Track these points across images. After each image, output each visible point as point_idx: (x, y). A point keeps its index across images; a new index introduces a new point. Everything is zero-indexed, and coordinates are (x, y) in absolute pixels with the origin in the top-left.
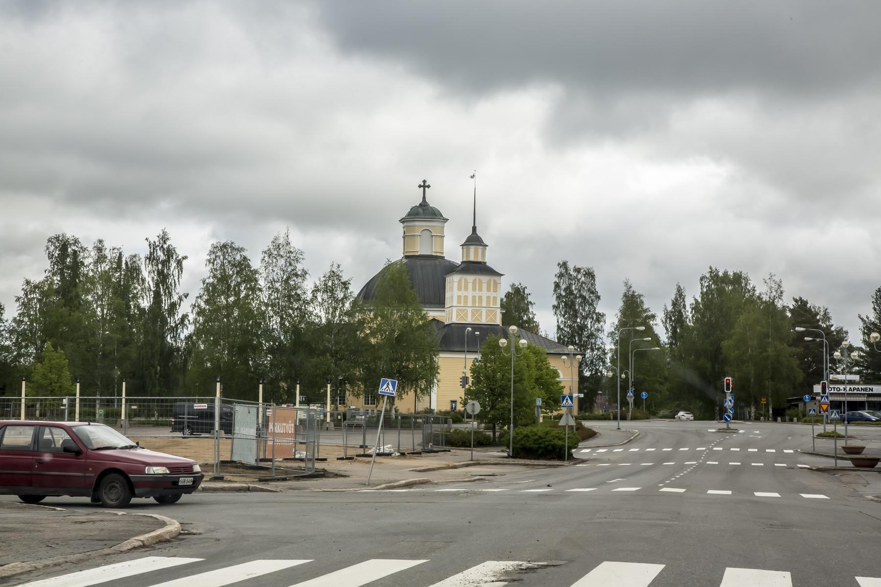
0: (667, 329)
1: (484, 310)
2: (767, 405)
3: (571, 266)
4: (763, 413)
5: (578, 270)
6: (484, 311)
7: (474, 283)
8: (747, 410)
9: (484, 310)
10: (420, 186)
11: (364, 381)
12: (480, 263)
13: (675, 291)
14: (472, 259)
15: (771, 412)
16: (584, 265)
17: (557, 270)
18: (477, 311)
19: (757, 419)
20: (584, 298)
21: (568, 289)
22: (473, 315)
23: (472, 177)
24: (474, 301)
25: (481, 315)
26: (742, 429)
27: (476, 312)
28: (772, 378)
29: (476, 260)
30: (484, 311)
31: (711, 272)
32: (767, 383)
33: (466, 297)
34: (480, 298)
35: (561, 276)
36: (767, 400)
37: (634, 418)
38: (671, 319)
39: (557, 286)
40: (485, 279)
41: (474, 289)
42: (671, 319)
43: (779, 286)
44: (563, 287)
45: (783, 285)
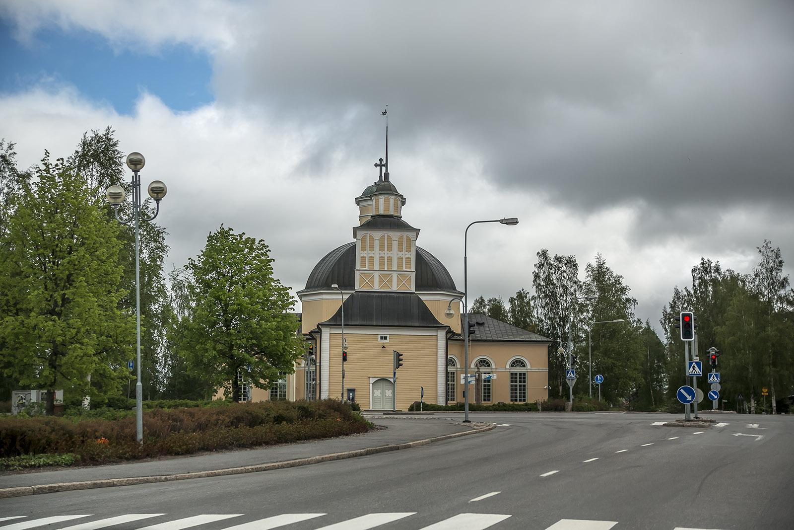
0: (666, 330)
1: (395, 275)
2: (769, 398)
3: (551, 255)
4: (764, 409)
5: (559, 259)
6: (395, 276)
7: (382, 240)
8: (746, 406)
9: (395, 275)
10: (376, 165)
11: (57, 346)
12: (392, 216)
13: (673, 294)
14: (381, 212)
15: (774, 404)
16: (565, 254)
17: (537, 260)
18: (386, 276)
19: (759, 411)
20: (565, 288)
21: (548, 280)
22: (381, 281)
23: (384, 114)
24: (382, 264)
25: (391, 281)
26: (723, 421)
27: (385, 277)
28: (774, 364)
29: (387, 213)
30: (395, 276)
31: (703, 264)
32: (768, 369)
33: (372, 258)
34: (390, 259)
35: (541, 266)
36: (769, 392)
37: (577, 409)
38: (670, 321)
39: (537, 276)
40: (395, 235)
41: (382, 249)
42: (670, 321)
43: (778, 256)
44: (542, 276)
45: (782, 253)
